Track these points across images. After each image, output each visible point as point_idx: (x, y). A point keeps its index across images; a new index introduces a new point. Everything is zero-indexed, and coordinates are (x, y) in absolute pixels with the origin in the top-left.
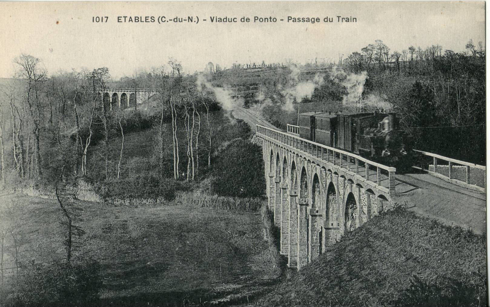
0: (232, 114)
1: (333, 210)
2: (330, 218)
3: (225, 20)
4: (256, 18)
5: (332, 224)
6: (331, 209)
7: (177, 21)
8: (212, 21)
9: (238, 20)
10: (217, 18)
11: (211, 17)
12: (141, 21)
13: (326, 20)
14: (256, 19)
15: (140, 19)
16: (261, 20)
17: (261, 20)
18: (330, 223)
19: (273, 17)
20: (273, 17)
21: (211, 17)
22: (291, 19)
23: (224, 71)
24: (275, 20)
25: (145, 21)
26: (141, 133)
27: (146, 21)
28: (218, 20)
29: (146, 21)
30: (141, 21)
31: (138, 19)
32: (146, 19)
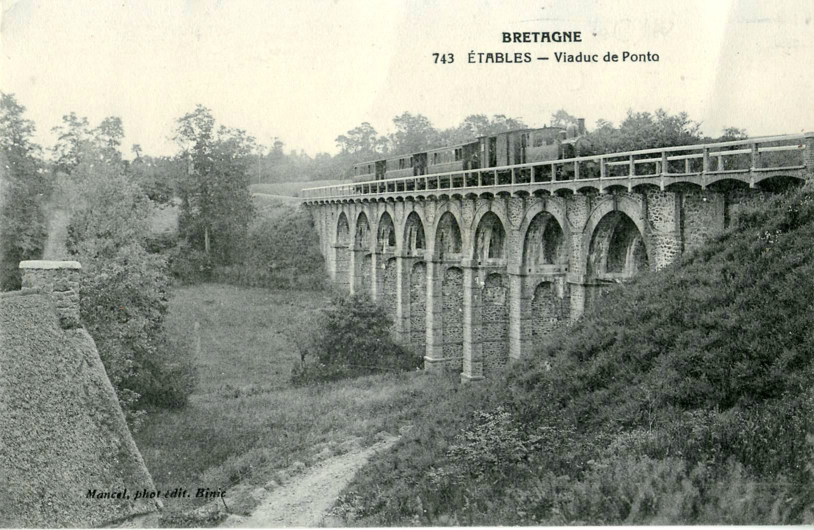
0: (541, 204)
1: (532, 251)
2: (527, 262)
3: (579, 59)
4: (626, 55)
5: (530, 270)
6: (529, 251)
7: (581, 61)
8: (558, 60)
9: (600, 59)
10: (567, 55)
11: (556, 53)
12: (507, 61)
13: (607, 58)
14: (625, 55)
15: (504, 57)
16: (634, 58)
17: (634, 58)
18: (528, 268)
19: (652, 53)
20: (652, 53)
21: (556, 53)
22: (577, 58)
23: (317, 160)
24: (655, 58)
25: (514, 60)
26: (630, 515)
27: (516, 61)
28: (567, 58)
29: (516, 61)
30: (507, 61)
31: (501, 57)
32: (516, 57)
